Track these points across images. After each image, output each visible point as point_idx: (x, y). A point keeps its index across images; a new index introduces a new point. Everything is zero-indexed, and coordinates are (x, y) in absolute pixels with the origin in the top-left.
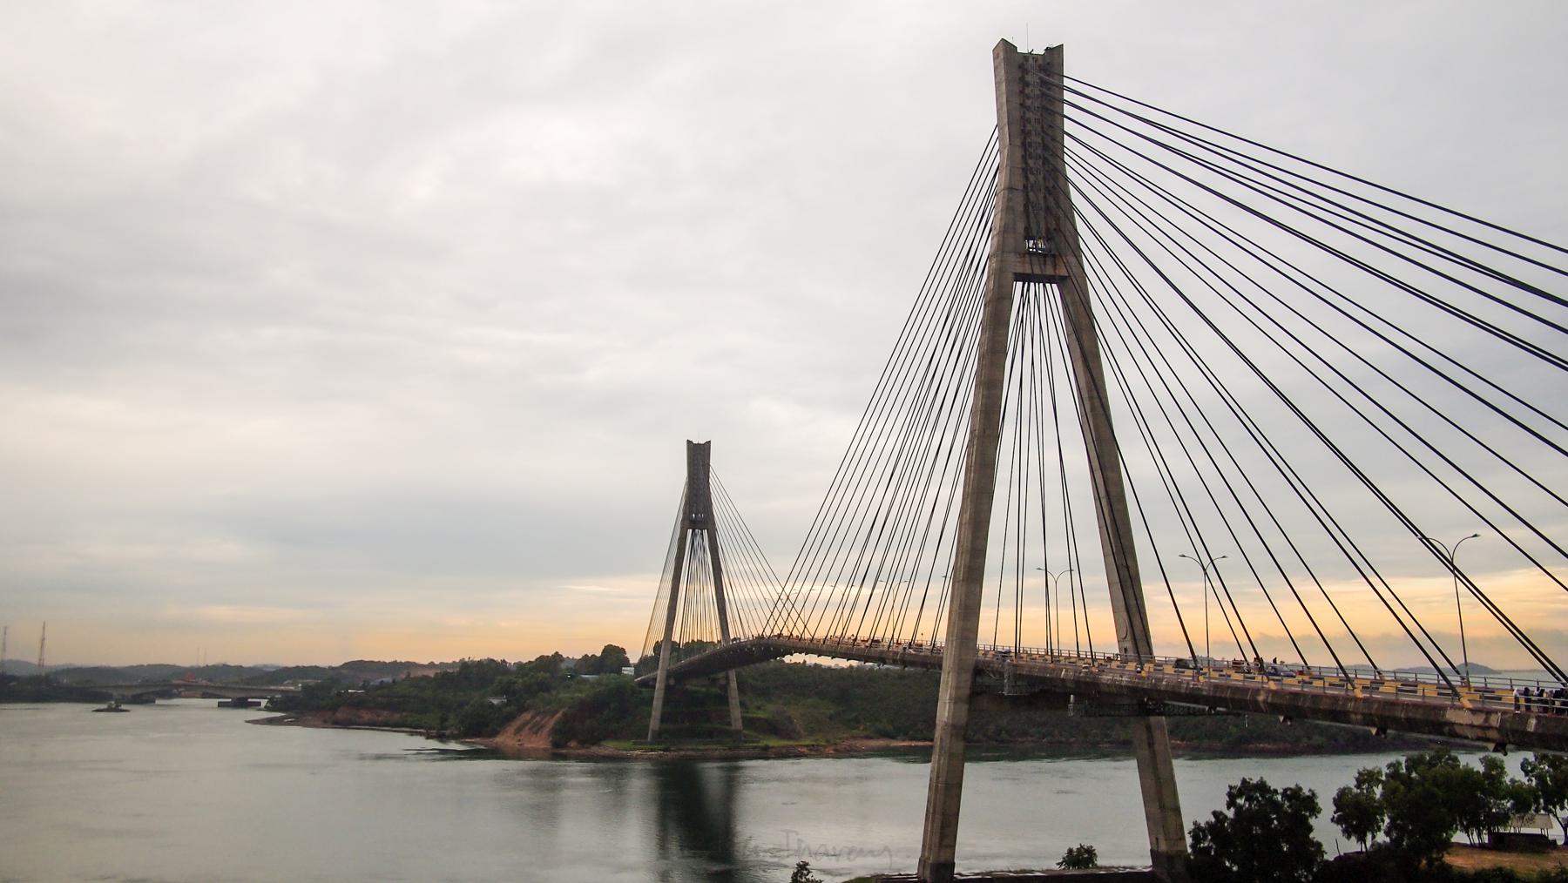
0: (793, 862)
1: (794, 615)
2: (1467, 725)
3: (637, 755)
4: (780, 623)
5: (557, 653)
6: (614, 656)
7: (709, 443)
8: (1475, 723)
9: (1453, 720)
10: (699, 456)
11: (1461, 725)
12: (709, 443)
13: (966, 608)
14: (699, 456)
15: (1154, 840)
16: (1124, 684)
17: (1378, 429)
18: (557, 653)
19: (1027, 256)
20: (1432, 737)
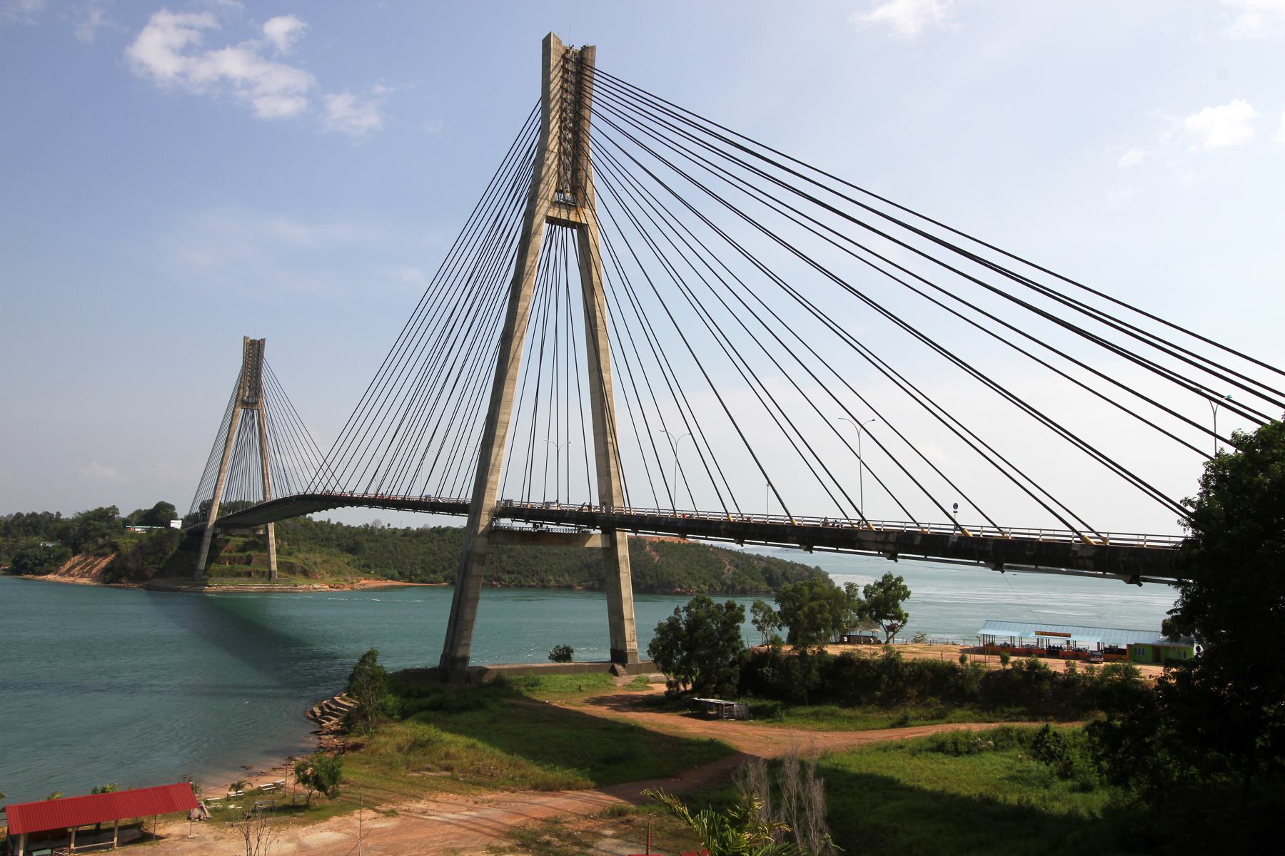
0: (365, 648)
1: (329, 474)
2: (872, 541)
3: (184, 588)
4: (333, 482)
5: (114, 506)
6: (161, 513)
7: (264, 340)
8: (879, 540)
9: (863, 538)
10: (254, 351)
11: (868, 541)
12: (264, 340)
13: (265, 497)
14: (254, 351)
15: (614, 642)
16: (616, 520)
17: (726, 285)
18: (114, 506)
19: (557, 205)
20: (727, 702)
